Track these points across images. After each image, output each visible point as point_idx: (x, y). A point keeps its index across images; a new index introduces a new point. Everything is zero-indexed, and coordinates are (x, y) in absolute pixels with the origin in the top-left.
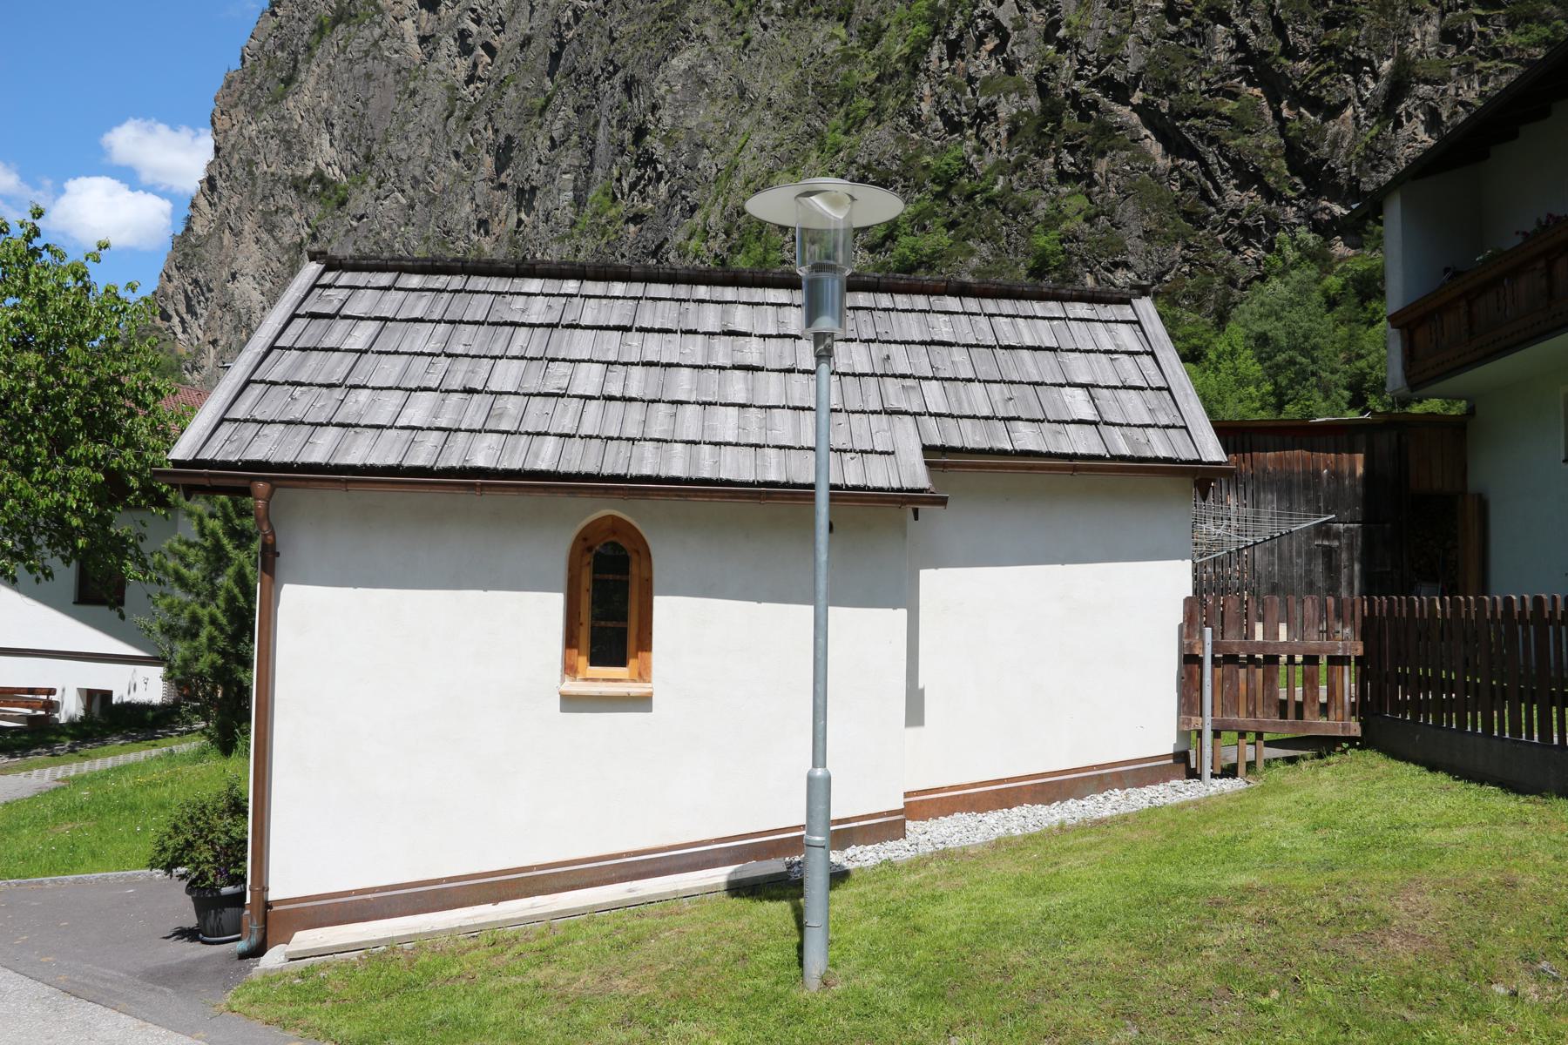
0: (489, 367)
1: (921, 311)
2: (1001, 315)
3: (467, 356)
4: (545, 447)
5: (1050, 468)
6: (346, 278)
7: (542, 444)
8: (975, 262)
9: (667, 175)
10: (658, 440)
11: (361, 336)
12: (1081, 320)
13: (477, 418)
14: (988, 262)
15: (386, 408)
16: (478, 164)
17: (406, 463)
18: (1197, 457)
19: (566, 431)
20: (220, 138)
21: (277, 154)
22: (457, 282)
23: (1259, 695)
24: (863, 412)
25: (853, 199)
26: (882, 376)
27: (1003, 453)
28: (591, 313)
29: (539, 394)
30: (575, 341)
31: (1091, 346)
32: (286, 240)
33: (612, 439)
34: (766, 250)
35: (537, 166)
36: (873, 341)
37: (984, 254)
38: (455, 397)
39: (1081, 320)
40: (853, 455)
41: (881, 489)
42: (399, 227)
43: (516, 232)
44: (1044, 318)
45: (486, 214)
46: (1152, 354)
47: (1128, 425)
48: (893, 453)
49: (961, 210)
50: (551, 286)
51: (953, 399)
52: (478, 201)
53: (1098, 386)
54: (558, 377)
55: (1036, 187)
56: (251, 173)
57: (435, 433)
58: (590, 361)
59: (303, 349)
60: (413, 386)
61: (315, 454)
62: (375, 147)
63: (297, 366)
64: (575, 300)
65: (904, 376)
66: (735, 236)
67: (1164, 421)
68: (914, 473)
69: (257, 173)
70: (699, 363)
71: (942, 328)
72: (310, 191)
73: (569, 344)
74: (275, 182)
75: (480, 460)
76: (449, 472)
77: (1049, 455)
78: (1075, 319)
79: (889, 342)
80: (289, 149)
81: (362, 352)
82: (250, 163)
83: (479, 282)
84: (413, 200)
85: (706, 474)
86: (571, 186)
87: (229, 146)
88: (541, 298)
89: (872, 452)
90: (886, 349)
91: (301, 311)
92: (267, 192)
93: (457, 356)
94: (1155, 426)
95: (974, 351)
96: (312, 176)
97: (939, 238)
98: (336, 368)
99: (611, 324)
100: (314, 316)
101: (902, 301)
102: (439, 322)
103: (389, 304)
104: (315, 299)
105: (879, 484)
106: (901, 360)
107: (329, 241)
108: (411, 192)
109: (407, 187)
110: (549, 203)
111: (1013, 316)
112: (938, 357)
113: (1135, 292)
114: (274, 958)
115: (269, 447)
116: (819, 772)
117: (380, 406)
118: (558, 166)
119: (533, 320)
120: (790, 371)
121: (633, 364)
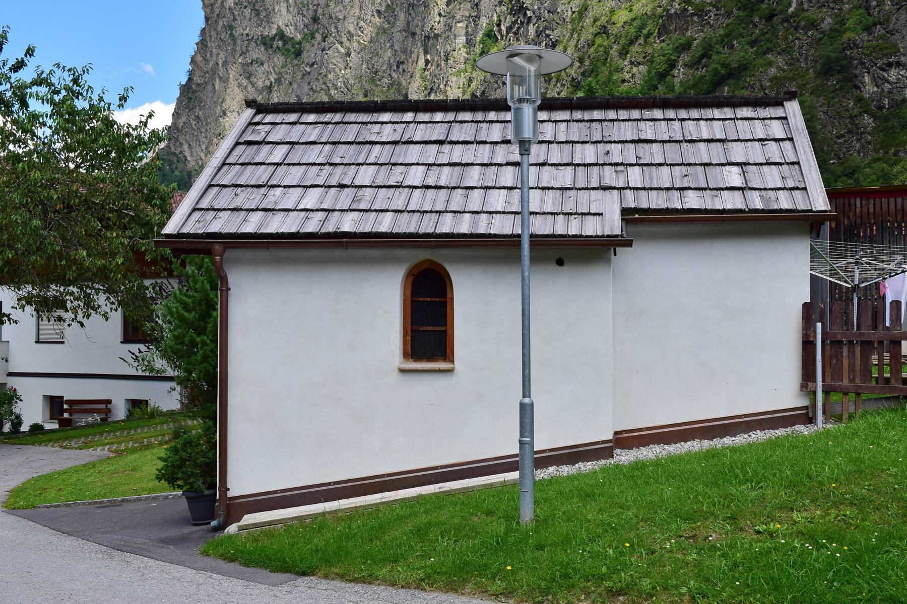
0: (356, 171)
1: (635, 120)
2: (689, 119)
3: (342, 164)
4: (386, 218)
5: (706, 219)
6: (269, 118)
7: (384, 217)
8: (773, 71)
9: (534, 20)
10: (455, 212)
11: (278, 154)
12: (746, 119)
13: (346, 203)
14: (784, 70)
15: (290, 199)
16: (395, 19)
17: (302, 231)
18: (810, 208)
19: (399, 209)
20: (208, 10)
21: (250, 20)
22: (338, 117)
23: (858, 368)
24: (587, 189)
25: (540, 57)
26: (603, 165)
27: (676, 211)
28: (420, 133)
29: (384, 187)
30: (409, 151)
31: (749, 137)
32: (260, 84)
33: (426, 212)
34: (610, 73)
35: (437, 19)
36: (600, 142)
37: (780, 64)
38: (333, 190)
39: (746, 119)
40: (576, 216)
41: (591, 237)
42: (340, 70)
43: (425, 70)
44: (719, 119)
45: (403, 57)
46: (791, 139)
47: (765, 189)
48: (602, 214)
49: (762, 30)
50: (396, 117)
51: (647, 177)
52: (396, 47)
53: (749, 164)
54: (397, 175)
55: (824, 6)
56: (231, 35)
57: (320, 213)
58: (418, 164)
59: (242, 164)
60: (308, 184)
61: (248, 228)
62: (320, 11)
63: (240, 175)
64: (412, 125)
65: (617, 164)
66: (587, 63)
67: (791, 184)
68: (612, 225)
69: (237, 34)
70: (485, 162)
71: (648, 131)
72: (275, 46)
73: (406, 154)
74: (249, 41)
75: (346, 227)
76: (328, 235)
77: (706, 211)
78: (742, 119)
79: (610, 142)
80: (258, 15)
81: (278, 164)
82: (231, 28)
83: (351, 117)
84: (349, 49)
85: (482, 231)
86: (464, 31)
87: (215, 15)
88: (390, 125)
89: (589, 214)
90: (607, 147)
91: (241, 140)
92: (244, 49)
93: (336, 164)
94: (784, 189)
95: (667, 145)
96: (276, 35)
97: (739, 52)
98: (261, 175)
99: (432, 139)
100: (249, 143)
101: (623, 114)
102: (325, 143)
103: (295, 134)
104: (250, 132)
105: (590, 234)
106: (617, 154)
107: (291, 83)
108: (347, 44)
109: (344, 39)
110: (448, 46)
111: (698, 120)
112: (642, 150)
113: (787, 96)
114: (232, 529)
115: (220, 224)
116: (527, 400)
117: (288, 197)
118: (454, 17)
119: (384, 139)
120: (543, 164)
121: (444, 165)
